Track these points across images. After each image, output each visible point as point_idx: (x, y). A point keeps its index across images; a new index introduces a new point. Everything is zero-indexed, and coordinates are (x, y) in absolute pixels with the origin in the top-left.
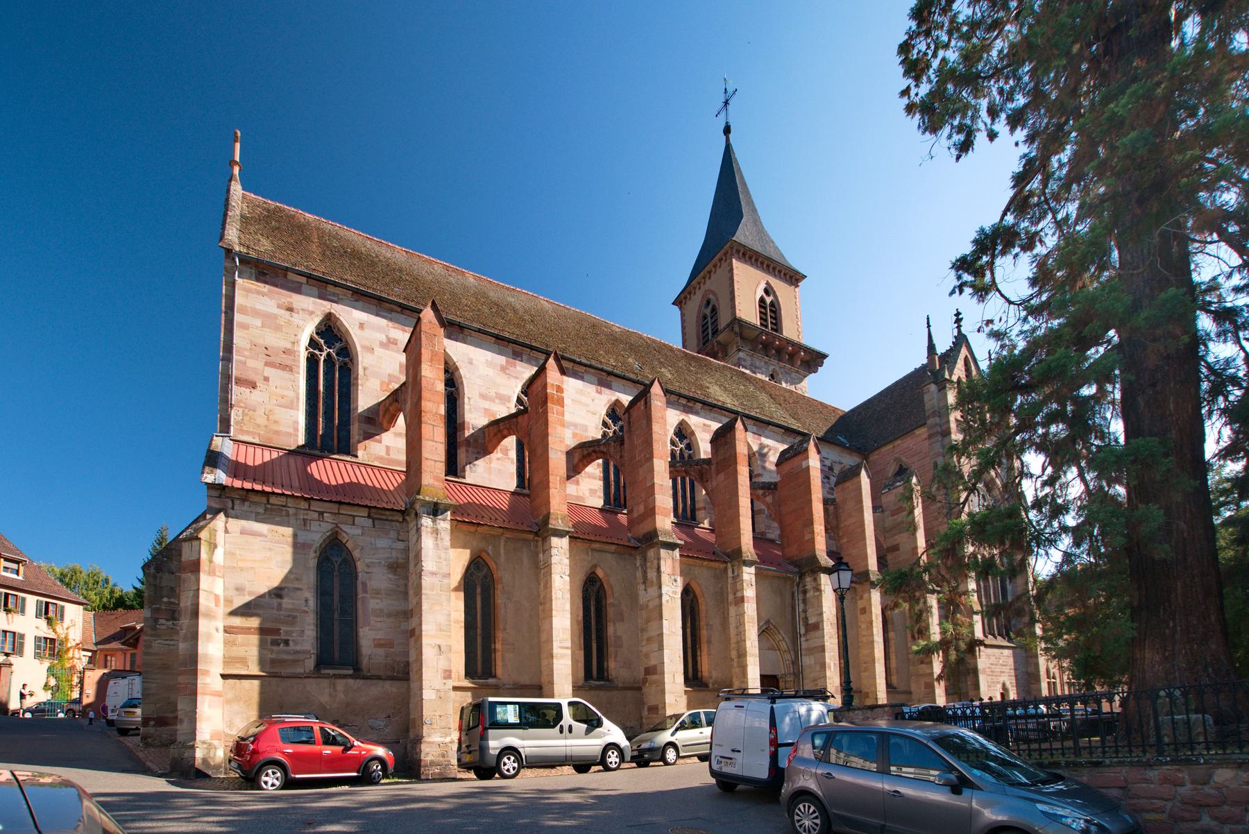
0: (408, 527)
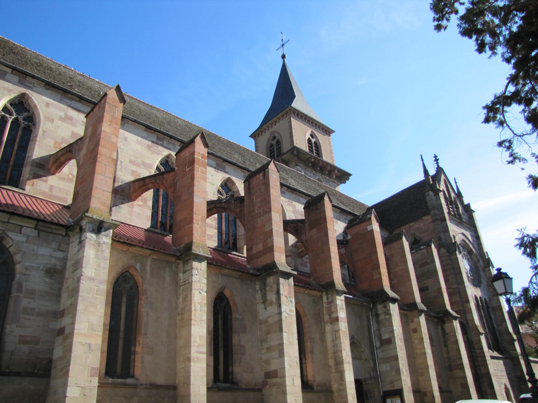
0: (69, 241)
